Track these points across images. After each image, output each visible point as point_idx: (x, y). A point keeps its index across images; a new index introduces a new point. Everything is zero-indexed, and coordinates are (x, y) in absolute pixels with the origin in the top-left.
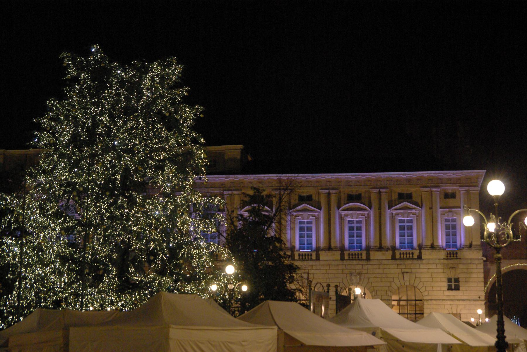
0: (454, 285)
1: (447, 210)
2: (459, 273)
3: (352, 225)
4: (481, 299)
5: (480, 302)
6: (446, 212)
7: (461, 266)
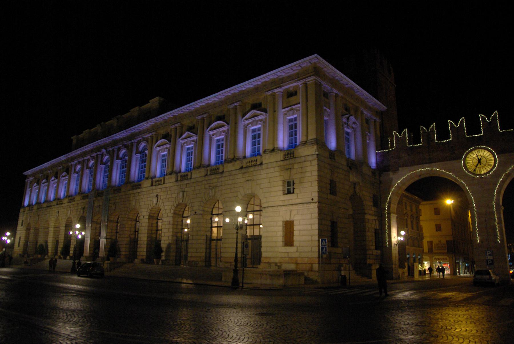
0: (290, 188)
1: (289, 108)
2: (296, 177)
4: (314, 201)
5: (312, 205)
6: (288, 111)
7: (296, 166)
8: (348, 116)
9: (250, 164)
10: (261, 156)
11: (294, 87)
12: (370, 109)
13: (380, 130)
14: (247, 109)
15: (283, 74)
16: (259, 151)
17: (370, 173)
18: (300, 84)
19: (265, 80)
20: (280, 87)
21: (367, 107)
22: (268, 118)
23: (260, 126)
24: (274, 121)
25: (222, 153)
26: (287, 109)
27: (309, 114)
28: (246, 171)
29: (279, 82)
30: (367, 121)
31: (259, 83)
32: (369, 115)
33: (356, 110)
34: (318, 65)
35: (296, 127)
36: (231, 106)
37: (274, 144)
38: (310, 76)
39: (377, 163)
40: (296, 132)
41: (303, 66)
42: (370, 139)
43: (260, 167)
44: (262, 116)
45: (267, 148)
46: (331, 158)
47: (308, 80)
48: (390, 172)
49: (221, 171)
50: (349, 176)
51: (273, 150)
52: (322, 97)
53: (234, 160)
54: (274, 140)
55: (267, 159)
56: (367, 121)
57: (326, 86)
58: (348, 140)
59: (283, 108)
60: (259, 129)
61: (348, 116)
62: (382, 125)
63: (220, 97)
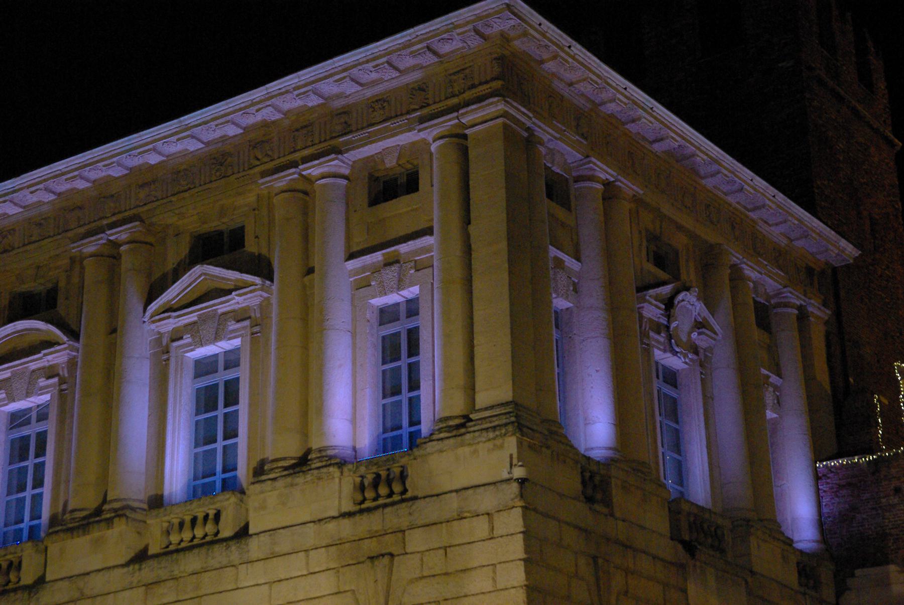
1: (377, 257)
3: (25, 431)
6: (376, 270)
7: (417, 541)
8: (666, 290)
9: (187, 535)
10: (243, 492)
11: (401, 149)
12: (779, 257)
13: (830, 357)
14: (171, 263)
15: (350, 88)
16: (230, 467)
17: (792, 578)
18: (430, 136)
19: (259, 117)
20: (338, 151)
21: (757, 246)
22: (274, 301)
23: (237, 342)
24: (305, 319)
25: (39, 482)
26: (368, 259)
27: (478, 285)
28: (163, 574)
29: (330, 129)
30: (764, 316)
31: (232, 131)
32: (771, 285)
33: (709, 259)
34: (517, 44)
35: (414, 348)
36: (91, 247)
37: (305, 435)
38: (479, 99)
39: (820, 523)
40: (413, 369)
41: (446, 48)
42: (779, 402)
43: (234, 553)
44: (250, 295)
45: (270, 454)
46: (590, 500)
47: (470, 116)
48: (892, 568)
49: (27, 578)
50: (684, 591)
51: (302, 463)
52: (541, 200)
53: (97, 517)
54: (306, 383)
55: (270, 508)
56: (764, 316)
57: (561, 149)
58: (673, 410)
59: (351, 256)
60: (231, 360)
61: (666, 290)
62: (839, 336)
63: (33, 199)
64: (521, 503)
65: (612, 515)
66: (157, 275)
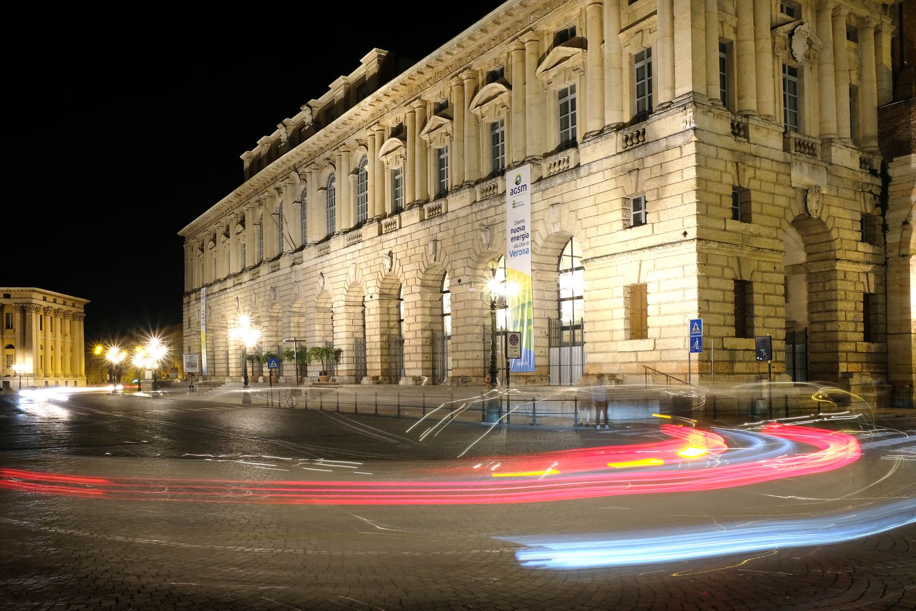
7: (650, 162)
8: (789, 27)
9: (557, 169)
49: (500, 192)
59: (622, 31)
61: (789, 27)
64: (695, 139)
65: (748, 142)
66: (541, 55)
